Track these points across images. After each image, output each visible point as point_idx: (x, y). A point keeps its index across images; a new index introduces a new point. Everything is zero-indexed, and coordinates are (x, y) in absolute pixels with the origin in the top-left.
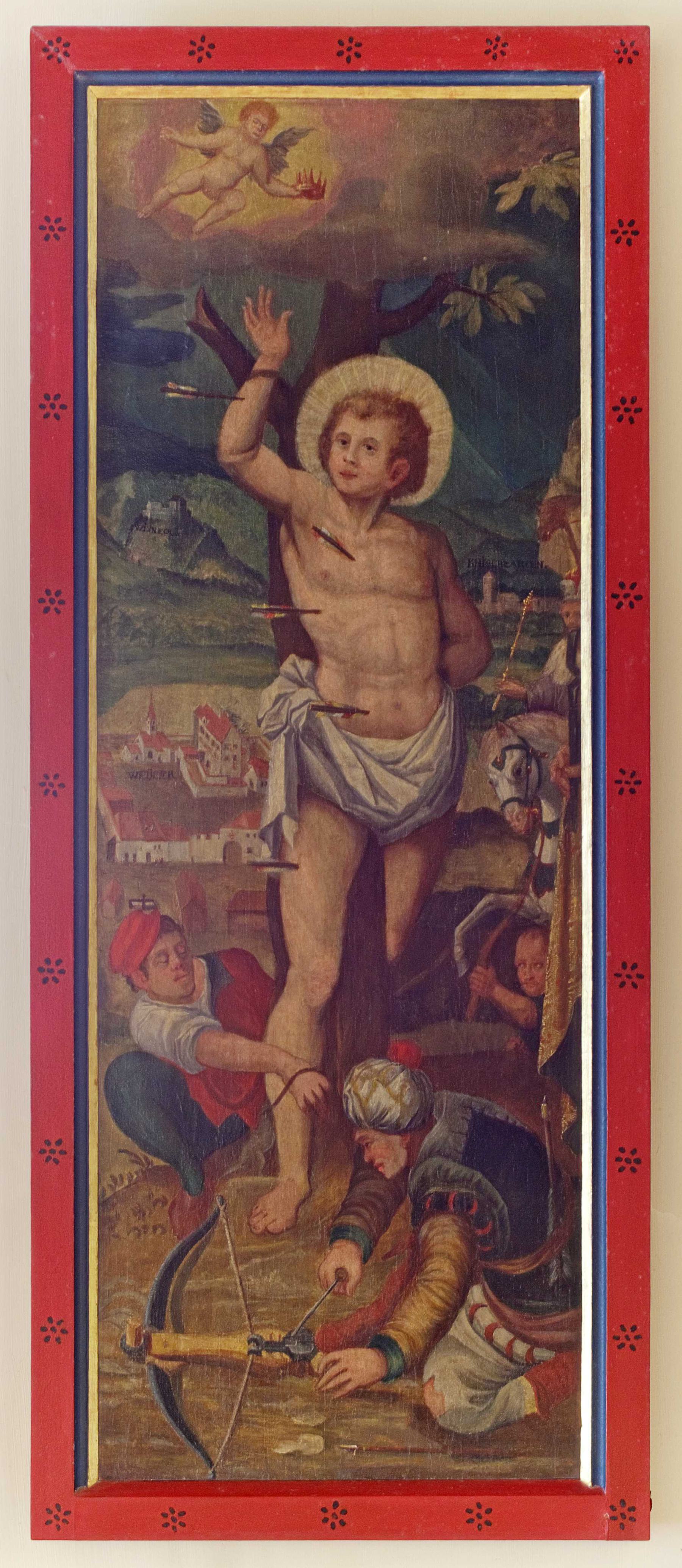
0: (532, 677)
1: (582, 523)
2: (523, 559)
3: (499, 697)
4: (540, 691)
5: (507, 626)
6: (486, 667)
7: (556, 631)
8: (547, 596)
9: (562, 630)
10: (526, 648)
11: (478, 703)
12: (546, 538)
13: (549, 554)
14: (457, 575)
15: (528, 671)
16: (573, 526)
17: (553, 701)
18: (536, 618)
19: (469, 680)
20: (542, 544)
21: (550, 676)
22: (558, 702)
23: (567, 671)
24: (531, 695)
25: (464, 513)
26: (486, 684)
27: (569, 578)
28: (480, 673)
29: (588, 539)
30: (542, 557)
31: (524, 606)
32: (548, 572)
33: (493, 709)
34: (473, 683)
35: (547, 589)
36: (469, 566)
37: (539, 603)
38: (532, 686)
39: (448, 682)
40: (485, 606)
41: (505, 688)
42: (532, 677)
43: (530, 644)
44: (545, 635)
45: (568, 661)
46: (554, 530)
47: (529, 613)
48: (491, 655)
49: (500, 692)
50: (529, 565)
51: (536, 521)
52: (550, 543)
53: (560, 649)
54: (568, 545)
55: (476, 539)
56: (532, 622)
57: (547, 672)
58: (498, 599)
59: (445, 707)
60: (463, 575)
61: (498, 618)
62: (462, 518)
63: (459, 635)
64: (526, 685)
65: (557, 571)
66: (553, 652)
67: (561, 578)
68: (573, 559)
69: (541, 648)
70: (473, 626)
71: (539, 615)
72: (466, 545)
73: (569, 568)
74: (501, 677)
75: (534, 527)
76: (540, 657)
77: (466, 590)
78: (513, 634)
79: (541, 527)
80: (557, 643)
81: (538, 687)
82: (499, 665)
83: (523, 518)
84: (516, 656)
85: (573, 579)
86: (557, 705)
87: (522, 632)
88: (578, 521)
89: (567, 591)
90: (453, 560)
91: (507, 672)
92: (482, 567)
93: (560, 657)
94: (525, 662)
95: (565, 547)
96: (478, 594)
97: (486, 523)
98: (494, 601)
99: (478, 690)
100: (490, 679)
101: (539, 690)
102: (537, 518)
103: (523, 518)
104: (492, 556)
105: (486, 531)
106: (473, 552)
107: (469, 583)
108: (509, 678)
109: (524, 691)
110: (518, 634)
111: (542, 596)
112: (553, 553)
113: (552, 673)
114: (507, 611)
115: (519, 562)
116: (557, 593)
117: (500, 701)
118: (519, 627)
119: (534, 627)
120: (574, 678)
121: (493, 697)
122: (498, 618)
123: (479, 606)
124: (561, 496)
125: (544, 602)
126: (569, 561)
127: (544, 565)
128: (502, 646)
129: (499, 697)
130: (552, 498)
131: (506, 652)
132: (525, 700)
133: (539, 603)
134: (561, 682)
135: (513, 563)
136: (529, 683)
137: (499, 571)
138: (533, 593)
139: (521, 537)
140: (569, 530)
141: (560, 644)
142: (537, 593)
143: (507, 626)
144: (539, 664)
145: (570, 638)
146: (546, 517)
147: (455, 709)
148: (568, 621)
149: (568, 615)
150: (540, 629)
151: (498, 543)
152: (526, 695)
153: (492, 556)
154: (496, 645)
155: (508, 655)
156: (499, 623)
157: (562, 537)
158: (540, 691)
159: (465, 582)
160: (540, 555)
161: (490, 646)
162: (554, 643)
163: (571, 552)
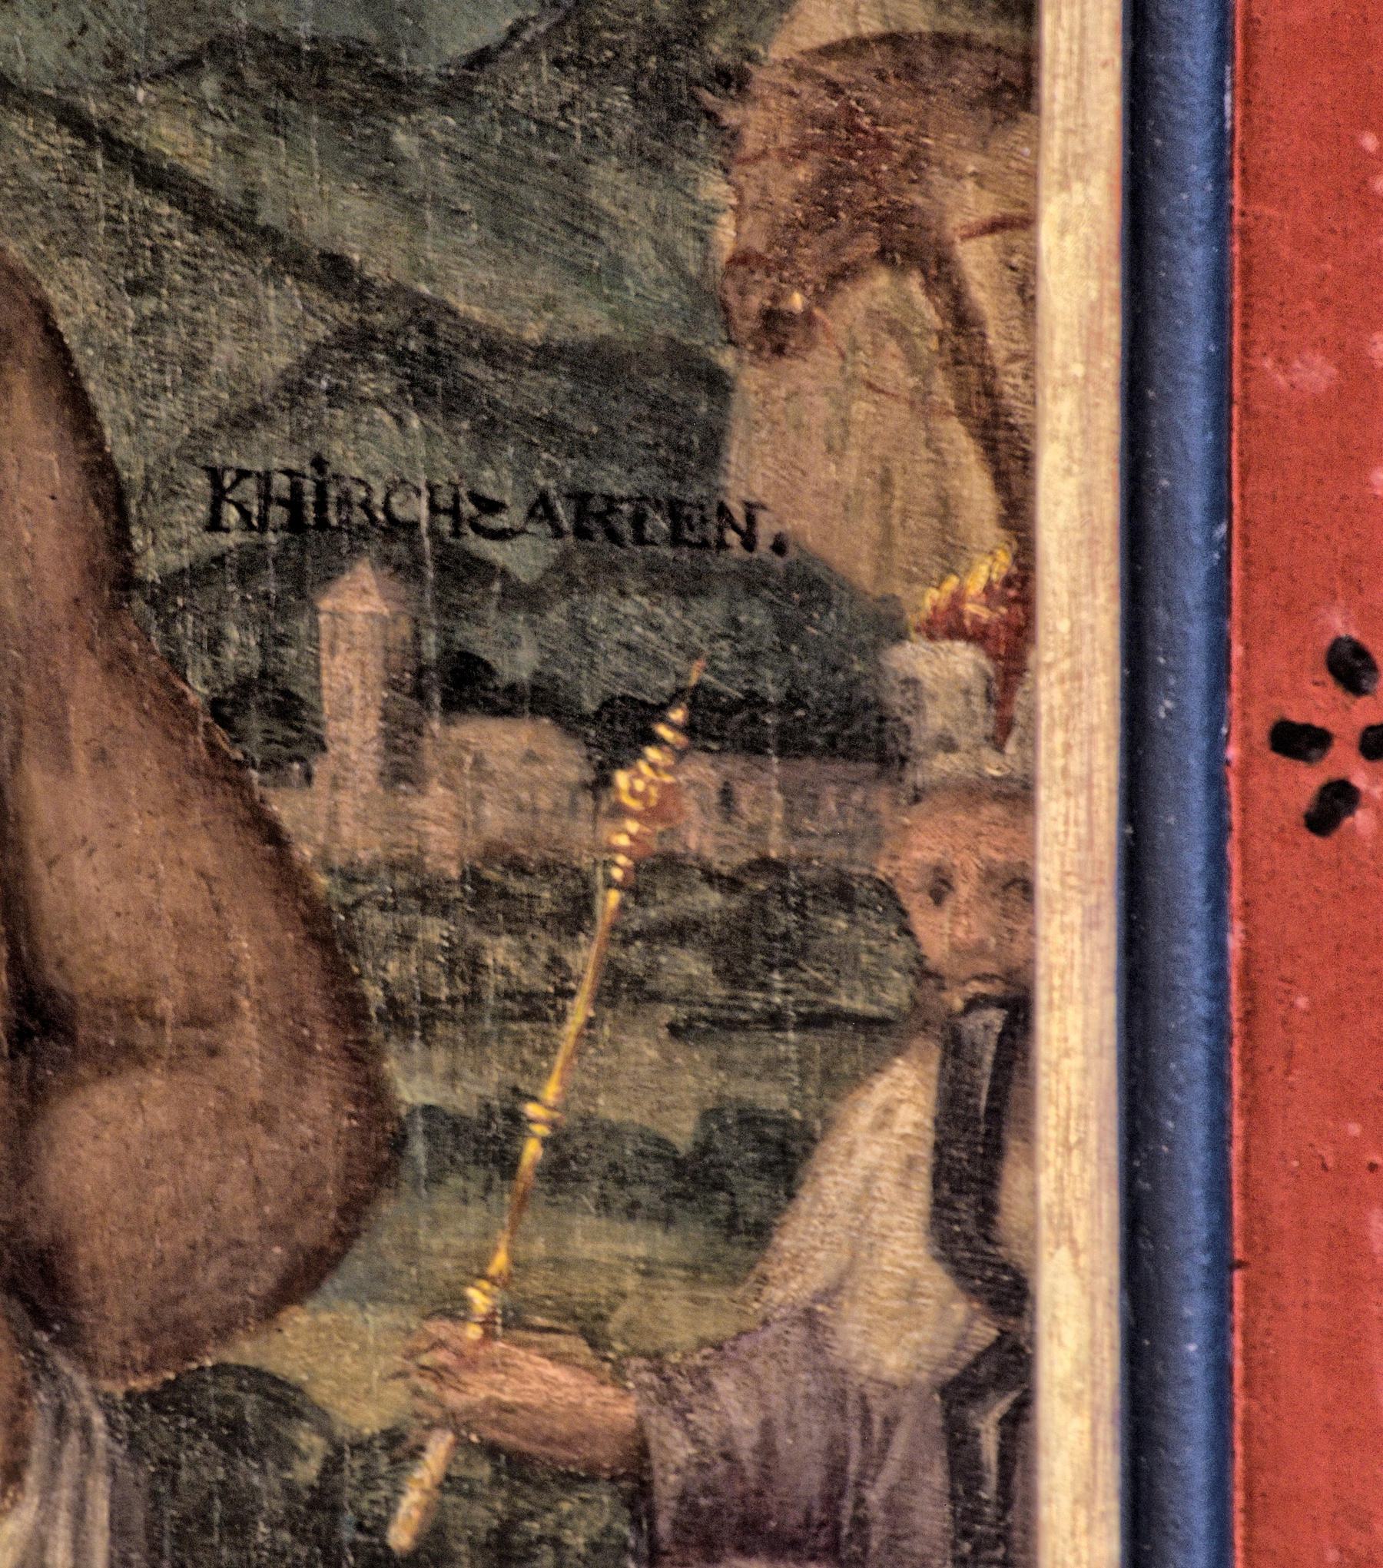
0: (682, 1320)
1: (1047, 235)
2: (611, 480)
3: (438, 1451)
4: (744, 1422)
5: (499, 951)
6: (345, 1238)
7: (859, 1005)
8: (792, 746)
9: (896, 993)
10: (637, 1116)
11: (290, 1490)
12: (776, 334)
13: (814, 449)
14: (126, 582)
15: (648, 1270)
16: (977, 261)
17: (831, 1501)
18: (711, 900)
19: (224, 1333)
20: (751, 378)
21: (809, 1318)
22: (873, 1497)
23: (937, 1281)
24: (673, 1451)
25: (170, 137)
26: (344, 1360)
27: (950, 625)
28: (305, 1278)
29: (1092, 343)
30: (748, 472)
31: (619, 812)
32: (800, 586)
33: (401, 1537)
34: (246, 1351)
35: (793, 700)
36: (214, 524)
37: (727, 796)
38: (674, 1383)
39: (71, 1339)
40: (336, 812)
41: (478, 1390)
42: (682, 1320)
43: (664, 1089)
44: (775, 1020)
45: (941, 1210)
46: (842, 275)
47: (660, 867)
48: (381, 1150)
49: (452, 1420)
50: (658, 524)
51: (707, 216)
52: (812, 372)
53: (885, 1124)
54: (941, 387)
55: (267, 330)
56: (679, 931)
57: (788, 1290)
58: (430, 760)
59: (47, 1517)
60: (173, 582)
61: (427, 896)
62: (155, 176)
63: (139, 1008)
64: (638, 1369)
65: (864, 572)
66: (832, 1148)
67: (890, 627)
68: (977, 491)
69: (750, 1119)
70: (254, 942)
71: (731, 884)
72: (195, 363)
73: (951, 554)
74: (455, 1308)
75: (688, 249)
76: (734, 1183)
77: (197, 692)
78: (538, 1008)
79: (742, 259)
80: (858, 1080)
81: (724, 1385)
82: (437, 1224)
83: (610, 184)
84: (560, 1170)
85: (978, 636)
86: (861, 1523)
87: (607, 995)
88: (1015, 223)
89: (935, 719)
90: (101, 470)
91: (504, 1282)
92: (312, 529)
93: (886, 1184)
94: (632, 1210)
95: (921, 404)
96: (271, 717)
97: (342, 216)
98: (401, 769)
99: (284, 1399)
100: (376, 1322)
101: (734, 1409)
102: (714, 189)
103: (610, 184)
104: (386, 451)
105: (336, 273)
106: (245, 420)
107: (215, 643)
108: (511, 1320)
109: (626, 1411)
110: (579, 1010)
111: (754, 748)
112: (833, 451)
113: (830, 1293)
114: (492, 852)
115: (580, 499)
116: (857, 733)
117: (449, 1483)
118: (585, 959)
119: (688, 965)
120: (985, 1332)
121: (398, 1446)
122: (427, 896)
123: (286, 807)
124: (894, 40)
125: (765, 790)
126: (946, 509)
127: (766, 529)
128: (462, 1100)
129: (438, 1451)
130: (828, 51)
131: (484, 1145)
132: (633, 1475)
133: (727, 796)
134: (894, 1362)
135: (541, 508)
136: (656, 1359)
137: (446, 566)
138: (689, 729)
139: (588, 320)
140: (942, 274)
141: (881, 1090)
142: (722, 723)
143: (499, 951)
144: (731, 1225)
145: (955, 1047)
146: (782, 194)
147: (119, 1529)
148: (939, 933)
149: (940, 887)
150: (732, 976)
151: (432, 360)
152: (639, 1453)
153: (386, 451)
154: (415, 1082)
155: (507, 1164)
156: (434, 930)
157: (897, 330)
158: (744, 1422)
159: (187, 627)
160: (734, 454)
161: (371, 1094)
162: (839, 1082)
163: (960, 442)
